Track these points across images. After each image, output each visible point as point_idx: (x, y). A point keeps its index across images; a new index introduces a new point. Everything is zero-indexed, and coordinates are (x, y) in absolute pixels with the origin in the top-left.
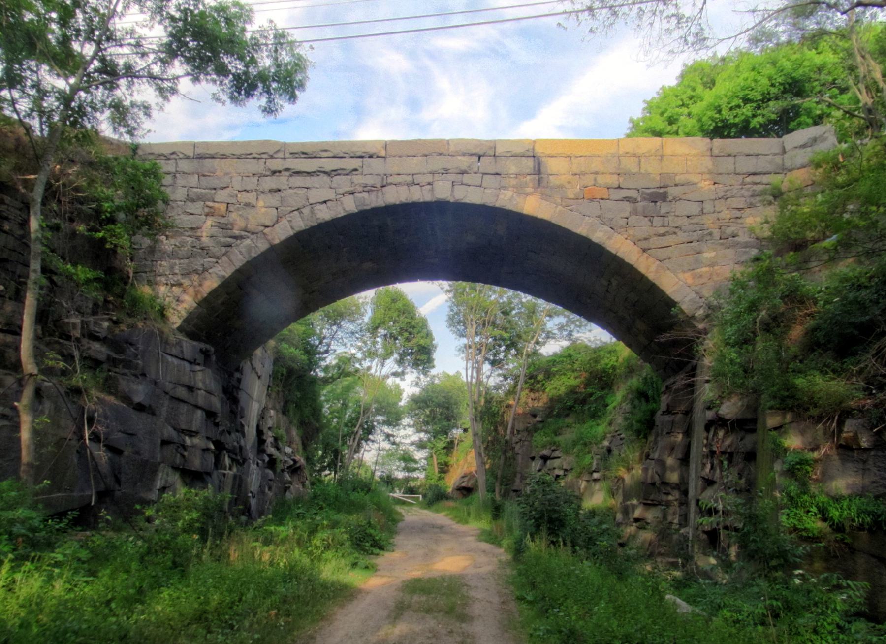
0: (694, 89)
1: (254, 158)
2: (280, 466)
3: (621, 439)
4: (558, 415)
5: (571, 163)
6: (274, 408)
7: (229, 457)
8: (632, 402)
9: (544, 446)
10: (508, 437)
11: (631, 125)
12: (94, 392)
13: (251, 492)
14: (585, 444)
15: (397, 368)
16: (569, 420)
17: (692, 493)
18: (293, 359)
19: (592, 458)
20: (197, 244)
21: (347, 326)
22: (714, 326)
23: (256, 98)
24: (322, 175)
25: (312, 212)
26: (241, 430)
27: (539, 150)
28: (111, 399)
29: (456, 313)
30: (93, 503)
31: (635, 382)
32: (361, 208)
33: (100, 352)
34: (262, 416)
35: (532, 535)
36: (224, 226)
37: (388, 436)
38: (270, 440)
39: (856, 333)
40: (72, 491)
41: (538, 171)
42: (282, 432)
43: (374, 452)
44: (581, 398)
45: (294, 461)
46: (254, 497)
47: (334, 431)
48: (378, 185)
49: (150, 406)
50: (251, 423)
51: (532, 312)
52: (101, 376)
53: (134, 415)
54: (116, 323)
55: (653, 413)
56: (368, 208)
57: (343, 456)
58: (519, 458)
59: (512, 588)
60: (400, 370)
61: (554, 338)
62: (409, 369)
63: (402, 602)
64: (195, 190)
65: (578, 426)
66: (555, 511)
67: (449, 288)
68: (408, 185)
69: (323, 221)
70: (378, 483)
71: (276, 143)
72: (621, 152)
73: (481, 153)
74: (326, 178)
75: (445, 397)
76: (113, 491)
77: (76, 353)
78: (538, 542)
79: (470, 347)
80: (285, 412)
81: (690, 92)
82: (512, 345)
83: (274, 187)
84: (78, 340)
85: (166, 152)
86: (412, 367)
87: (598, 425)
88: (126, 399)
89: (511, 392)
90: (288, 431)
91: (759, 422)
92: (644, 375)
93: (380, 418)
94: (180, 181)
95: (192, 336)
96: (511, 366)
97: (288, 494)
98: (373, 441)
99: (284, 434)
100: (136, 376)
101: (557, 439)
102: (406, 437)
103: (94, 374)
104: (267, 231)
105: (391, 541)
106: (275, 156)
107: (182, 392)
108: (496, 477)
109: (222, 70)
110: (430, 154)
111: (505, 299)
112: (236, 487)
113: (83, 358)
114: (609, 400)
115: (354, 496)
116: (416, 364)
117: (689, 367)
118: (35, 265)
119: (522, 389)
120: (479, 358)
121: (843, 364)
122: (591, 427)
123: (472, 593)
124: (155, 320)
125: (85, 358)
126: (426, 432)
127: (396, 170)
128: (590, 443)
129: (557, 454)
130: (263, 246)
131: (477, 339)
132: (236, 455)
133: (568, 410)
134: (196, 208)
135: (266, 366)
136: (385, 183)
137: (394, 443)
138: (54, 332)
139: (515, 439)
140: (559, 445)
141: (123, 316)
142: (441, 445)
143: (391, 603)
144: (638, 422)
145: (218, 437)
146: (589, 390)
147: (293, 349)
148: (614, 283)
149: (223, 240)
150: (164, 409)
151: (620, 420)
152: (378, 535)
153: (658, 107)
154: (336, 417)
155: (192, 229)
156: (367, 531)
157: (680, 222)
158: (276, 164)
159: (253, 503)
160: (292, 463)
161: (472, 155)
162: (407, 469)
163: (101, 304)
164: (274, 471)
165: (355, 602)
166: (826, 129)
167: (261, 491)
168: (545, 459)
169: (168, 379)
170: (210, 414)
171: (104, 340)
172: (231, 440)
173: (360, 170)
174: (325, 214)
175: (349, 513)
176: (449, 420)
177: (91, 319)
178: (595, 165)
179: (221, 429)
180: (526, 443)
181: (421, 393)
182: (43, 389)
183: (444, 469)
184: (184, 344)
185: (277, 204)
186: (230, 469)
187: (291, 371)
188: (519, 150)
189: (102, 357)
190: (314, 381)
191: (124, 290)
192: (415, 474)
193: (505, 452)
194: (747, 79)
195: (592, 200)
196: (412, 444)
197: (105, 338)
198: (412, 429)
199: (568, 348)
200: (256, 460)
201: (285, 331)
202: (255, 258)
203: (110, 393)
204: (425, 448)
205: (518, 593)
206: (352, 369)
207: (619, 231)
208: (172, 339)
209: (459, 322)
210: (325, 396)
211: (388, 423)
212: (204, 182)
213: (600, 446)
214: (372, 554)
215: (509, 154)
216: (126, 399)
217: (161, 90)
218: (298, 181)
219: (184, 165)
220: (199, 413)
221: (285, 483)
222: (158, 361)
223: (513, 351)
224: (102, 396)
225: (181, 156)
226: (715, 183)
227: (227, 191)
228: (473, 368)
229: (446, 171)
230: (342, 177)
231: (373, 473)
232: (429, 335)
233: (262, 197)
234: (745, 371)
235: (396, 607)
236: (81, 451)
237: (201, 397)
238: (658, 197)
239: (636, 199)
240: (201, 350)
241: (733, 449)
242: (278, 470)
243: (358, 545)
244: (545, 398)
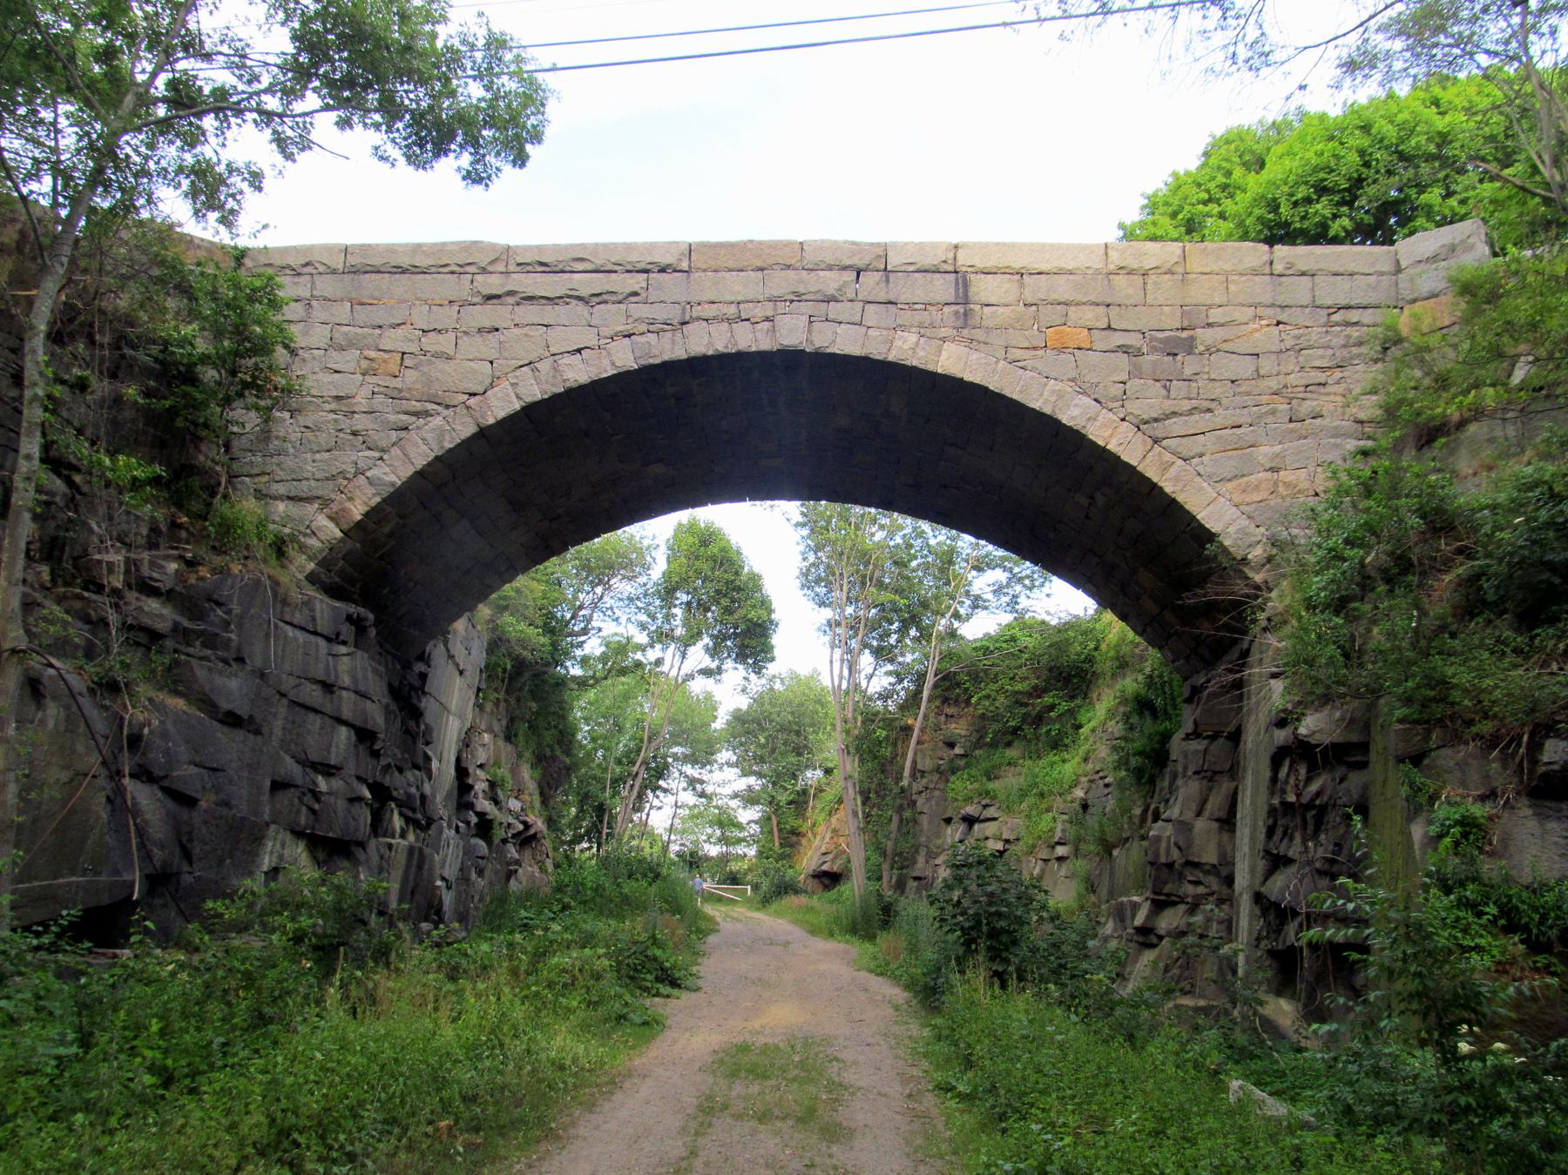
0: (1228, 174)
1: (452, 273)
2: (499, 833)
3: (1107, 786)
4: (994, 745)
5: (1022, 285)
6: (490, 730)
7: (401, 814)
8: (1127, 717)
9: (968, 800)
10: (905, 783)
11: (1121, 233)
12: (143, 690)
13: (443, 879)
14: (1042, 795)
15: (709, 662)
16: (1012, 753)
17: (1242, 880)
18: (523, 642)
19: (1054, 819)
20: (345, 423)
21: (621, 586)
22: (1284, 576)
23: (452, 155)
24: (574, 302)
25: (555, 368)
26: (423, 765)
28: (179, 703)
29: (813, 565)
30: (135, 897)
31: (1131, 684)
32: (643, 362)
33: (161, 616)
34: (466, 743)
35: (959, 961)
36: (395, 394)
37: (692, 782)
38: (480, 786)
39: (1557, 581)
40: (97, 874)
41: (963, 298)
42: (503, 772)
43: (668, 811)
44: (1034, 713)
45: (525, 823)
46: (449, 888)
47: (598, 773)
48: (675, 322)
49: (251, 717)
50: (445, 755)
51: (948, 558)
52: (161, 661)
53: (221, 734)
54: (191, 564)
55: (1166, 737)
56: (657, 361)
57: (612, 817)
59: (925, 1064)
60: (714, 665)
61: (986, 608)
63: (710, 1098)
64: (346, 329)
65: (1028, 762)
66: (999, 915)
67: (801, 519)
69: (575, 385)
70: (674, 864)
71: (493, 246)
72: (1112, 267)
73: (861, 263)
74: (580, 308)
75: (792, 713)
76: (178, 874)
77: (113, 618)
78: (969, 974)
79: (838, 624)
80: (509, 737)
81: (1221, 179)
82: (911, 620)
83: (487, 324)
84: (116, 592)
85: (294, 261)
86: (735, 661)
87: (1064, 761)
88: (207, 703)
90: (515, 771)
91: (1373, 747)
92: (1148, 670)
93: (677, 750)
94: (319, 313)
95: (333, 592)
96: (909, 658)
97: (512, 882)
98: (665, 791)
99: (508, 776)
100: (226, 662)
101: (991, 786)
102: (723, 783)
103: (146, 655)
104: (473, 401)
105: (694, 969)
106: (490, 269)
107: (313, 694)
108: (884, 854)
109: (391, 110)
110: (770, 267)
111: (898, 540)
112: (413, 869)
113: (126, 627)
114: (1082, 717)
115: (628, 887)
116: (741, 657)
117: (1234, 654)
118: (31, 446)
120: (854, 644)
121: (1532, 638)
122: (1052, 765)
123: (849, 1077)
124: (265, 561)
125: (131, 627)
126: (760, 775)
128: (1051, 793)
129: (991, 812)
130: (466, 430)
131: (850, 610)
132: (414, 810)
133: (1012, 735)
134: (348, 360)
135: (474, 652)
136: (687, 318)
137: (702, 795)
138: (74, 577)
139: (916, 787)
140: (993, 798)
141: (203, 552)
142: (783, 798)
143: (690, 1100)
144: (1140, 753)
145: (379, 778)
147: (522, 626)
148: (1100, 500)
149: (392, 418)
150: (278, 721)
151: (1103, 751)
152: (669, 958)
153: (1167, 204)
154: (602, 747)
155: (338, 398)
156: (649, 953)
157: (1218, 390)
158: (493, 284)
159: (448, 898)
160: (521, 827)
161: (845, 268)
162: (724, 840)
163: (164, 528)
164: (489, 841)
165: (618, 1096)
166: (1470, 231)
167: (463, 877)
168: (970, 821)
169: (287, 667)
170: (364, 735)
171: (169, 596)
172: (404, 783)
173: (644, 295)
174: (579, 373)
175: (621, 917)
176: (799, 754)
177: (145, 556)
178: (1063, 289)
179: (383, 762)
180: (936, 793)
181: (750, 707)
182: (45, 680)
183: (791, 839)
184: (318, 606)
185: (492, 354)
186: (403, 835)
187: (520, 665)
188: (928, 261)
189: (162, 626)
190: (561, 683)
191: (209, 505)
192: (740, 849)
193: (900, 809)
194: (1322, 154)
195: (1062, 349)
196: (735, 796)
197: (170, 591)
198: (736, 770)
199: (1009, 626)
200: (455, 821)
201: (508, 589)
202: (450, 450)
203: (177, 693)
204: (758, 803)
205: (938, 1076)
206: (628, 663)
207: (1111, 405)
208: (295, 596)
209: (818, 581)
210: (582, 709)
211: (693, 760)
212: (362, 314)
213: (1069, 798)
214: (658, 995)
215: (911, 268)
216: (207, 703)
217: (280, 142)
218: (529, 313)
219: (326, 286)
220: (343, 733)
221: (509, 864)
222: (267, 635)
223: (913, 632)
224: (161, 696)
225: (322, 269)
226: (1278, 323)
227: (400, 331)
228: (842, 661)
229: (798, 297)
230: (610, 306)
231: (665, 848)
232: (765, 604)
233: (465, 342)
234: (1346, 656)
235: (700, 1108)
236: (117, 800)
237: (347, 704)
238: (1178, 346)
239: (1139, 349)
240: (349, 618)
241: (1325, 798)
242: (496, 841)
243: (632, 978)
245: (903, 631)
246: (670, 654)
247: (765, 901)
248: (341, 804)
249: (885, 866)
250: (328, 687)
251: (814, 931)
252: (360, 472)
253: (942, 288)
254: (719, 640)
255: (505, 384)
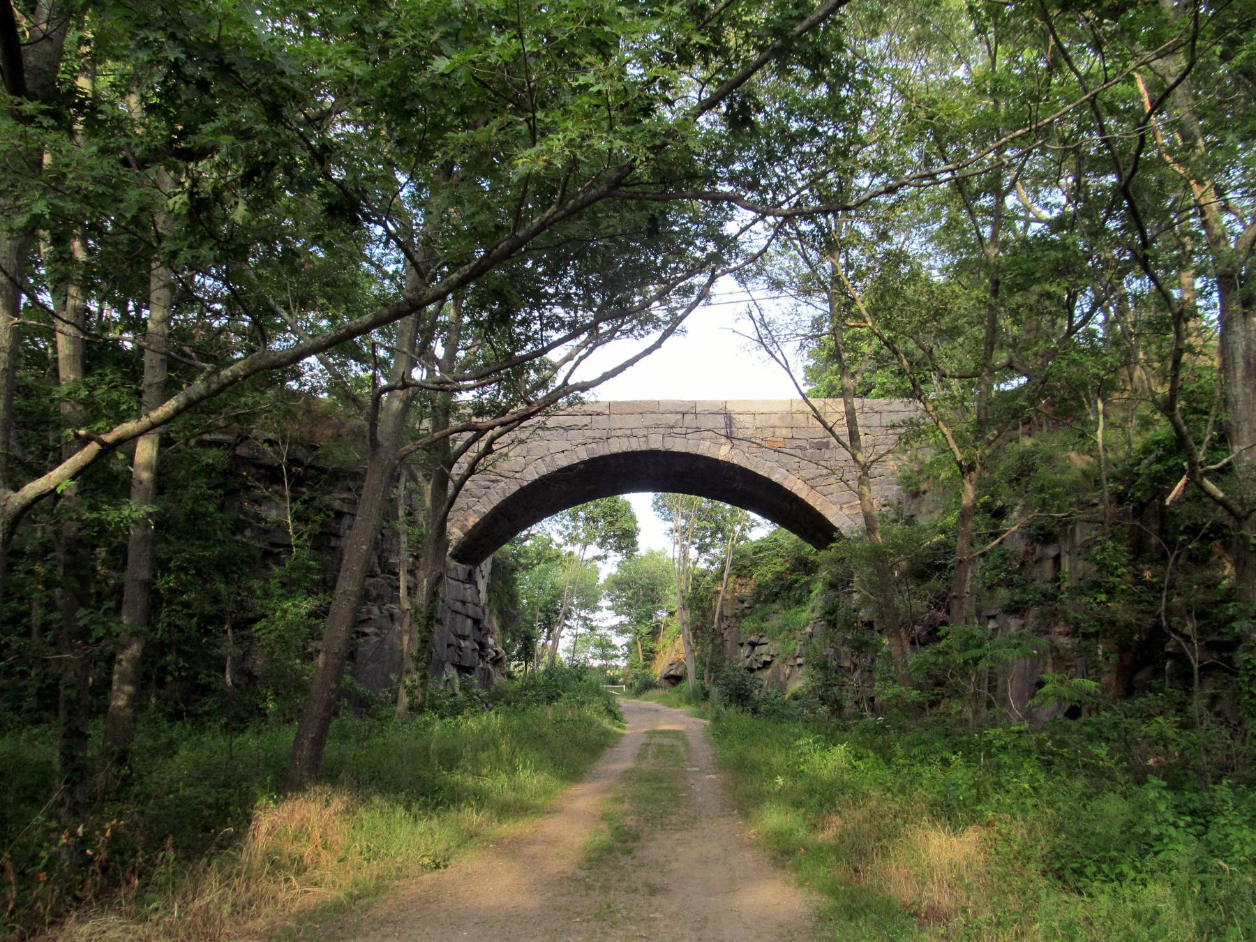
4: (765, 602)
9: (752, 633)
10: (715, 626)
14: (790, 630)
16: (775, 606)
27: (729, 408)
58: (728, 645)
62: (611, 553)
68: (628, 437)
89: (718, 578)
102: (604, 619)
104: (517, 475)
107: (458, 606)
119: (729, 575)
126: (629, 615)
127: (619, 425)
129: (764, 640)
130: (515, 488)
139: (723, 625)
142: (645, 630)
146: (794, 577)
162: (603, 657)
168: (753, 645)
174: (563, 461)
176: (653, 602)
178: (774, 420)
183: (650, 655)
185: (524, 454)
188: (714, 409)
196: (612, 628)
211: (584, 606)
220: (470, 622)
229: (658, 426)
232: (633, 518)
244: (752, 584)
245: (713, 535)
246: (577, 549)
247: (638, 694)
248: (469, 652)
249: (706, 671)
250: (464, 603)
251: (670, 706)
252: (469, 508)
253: (721, 421)
254: (604, 540)
255: (531, 467)
